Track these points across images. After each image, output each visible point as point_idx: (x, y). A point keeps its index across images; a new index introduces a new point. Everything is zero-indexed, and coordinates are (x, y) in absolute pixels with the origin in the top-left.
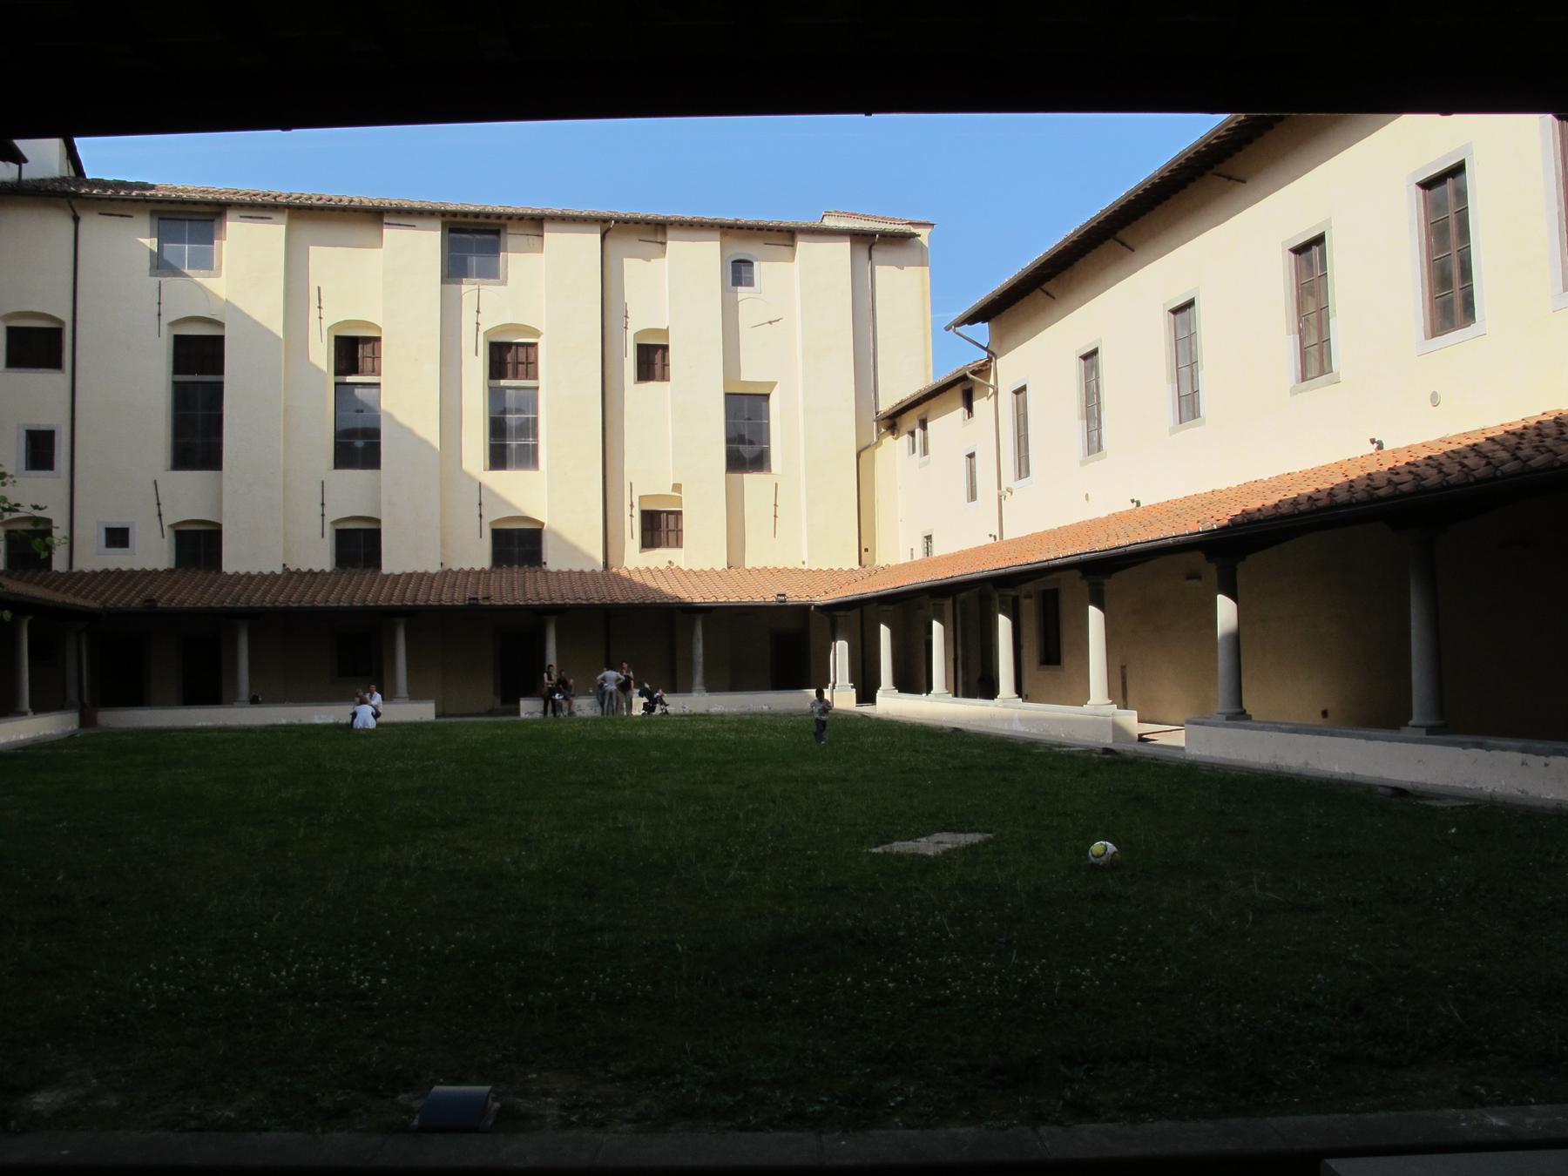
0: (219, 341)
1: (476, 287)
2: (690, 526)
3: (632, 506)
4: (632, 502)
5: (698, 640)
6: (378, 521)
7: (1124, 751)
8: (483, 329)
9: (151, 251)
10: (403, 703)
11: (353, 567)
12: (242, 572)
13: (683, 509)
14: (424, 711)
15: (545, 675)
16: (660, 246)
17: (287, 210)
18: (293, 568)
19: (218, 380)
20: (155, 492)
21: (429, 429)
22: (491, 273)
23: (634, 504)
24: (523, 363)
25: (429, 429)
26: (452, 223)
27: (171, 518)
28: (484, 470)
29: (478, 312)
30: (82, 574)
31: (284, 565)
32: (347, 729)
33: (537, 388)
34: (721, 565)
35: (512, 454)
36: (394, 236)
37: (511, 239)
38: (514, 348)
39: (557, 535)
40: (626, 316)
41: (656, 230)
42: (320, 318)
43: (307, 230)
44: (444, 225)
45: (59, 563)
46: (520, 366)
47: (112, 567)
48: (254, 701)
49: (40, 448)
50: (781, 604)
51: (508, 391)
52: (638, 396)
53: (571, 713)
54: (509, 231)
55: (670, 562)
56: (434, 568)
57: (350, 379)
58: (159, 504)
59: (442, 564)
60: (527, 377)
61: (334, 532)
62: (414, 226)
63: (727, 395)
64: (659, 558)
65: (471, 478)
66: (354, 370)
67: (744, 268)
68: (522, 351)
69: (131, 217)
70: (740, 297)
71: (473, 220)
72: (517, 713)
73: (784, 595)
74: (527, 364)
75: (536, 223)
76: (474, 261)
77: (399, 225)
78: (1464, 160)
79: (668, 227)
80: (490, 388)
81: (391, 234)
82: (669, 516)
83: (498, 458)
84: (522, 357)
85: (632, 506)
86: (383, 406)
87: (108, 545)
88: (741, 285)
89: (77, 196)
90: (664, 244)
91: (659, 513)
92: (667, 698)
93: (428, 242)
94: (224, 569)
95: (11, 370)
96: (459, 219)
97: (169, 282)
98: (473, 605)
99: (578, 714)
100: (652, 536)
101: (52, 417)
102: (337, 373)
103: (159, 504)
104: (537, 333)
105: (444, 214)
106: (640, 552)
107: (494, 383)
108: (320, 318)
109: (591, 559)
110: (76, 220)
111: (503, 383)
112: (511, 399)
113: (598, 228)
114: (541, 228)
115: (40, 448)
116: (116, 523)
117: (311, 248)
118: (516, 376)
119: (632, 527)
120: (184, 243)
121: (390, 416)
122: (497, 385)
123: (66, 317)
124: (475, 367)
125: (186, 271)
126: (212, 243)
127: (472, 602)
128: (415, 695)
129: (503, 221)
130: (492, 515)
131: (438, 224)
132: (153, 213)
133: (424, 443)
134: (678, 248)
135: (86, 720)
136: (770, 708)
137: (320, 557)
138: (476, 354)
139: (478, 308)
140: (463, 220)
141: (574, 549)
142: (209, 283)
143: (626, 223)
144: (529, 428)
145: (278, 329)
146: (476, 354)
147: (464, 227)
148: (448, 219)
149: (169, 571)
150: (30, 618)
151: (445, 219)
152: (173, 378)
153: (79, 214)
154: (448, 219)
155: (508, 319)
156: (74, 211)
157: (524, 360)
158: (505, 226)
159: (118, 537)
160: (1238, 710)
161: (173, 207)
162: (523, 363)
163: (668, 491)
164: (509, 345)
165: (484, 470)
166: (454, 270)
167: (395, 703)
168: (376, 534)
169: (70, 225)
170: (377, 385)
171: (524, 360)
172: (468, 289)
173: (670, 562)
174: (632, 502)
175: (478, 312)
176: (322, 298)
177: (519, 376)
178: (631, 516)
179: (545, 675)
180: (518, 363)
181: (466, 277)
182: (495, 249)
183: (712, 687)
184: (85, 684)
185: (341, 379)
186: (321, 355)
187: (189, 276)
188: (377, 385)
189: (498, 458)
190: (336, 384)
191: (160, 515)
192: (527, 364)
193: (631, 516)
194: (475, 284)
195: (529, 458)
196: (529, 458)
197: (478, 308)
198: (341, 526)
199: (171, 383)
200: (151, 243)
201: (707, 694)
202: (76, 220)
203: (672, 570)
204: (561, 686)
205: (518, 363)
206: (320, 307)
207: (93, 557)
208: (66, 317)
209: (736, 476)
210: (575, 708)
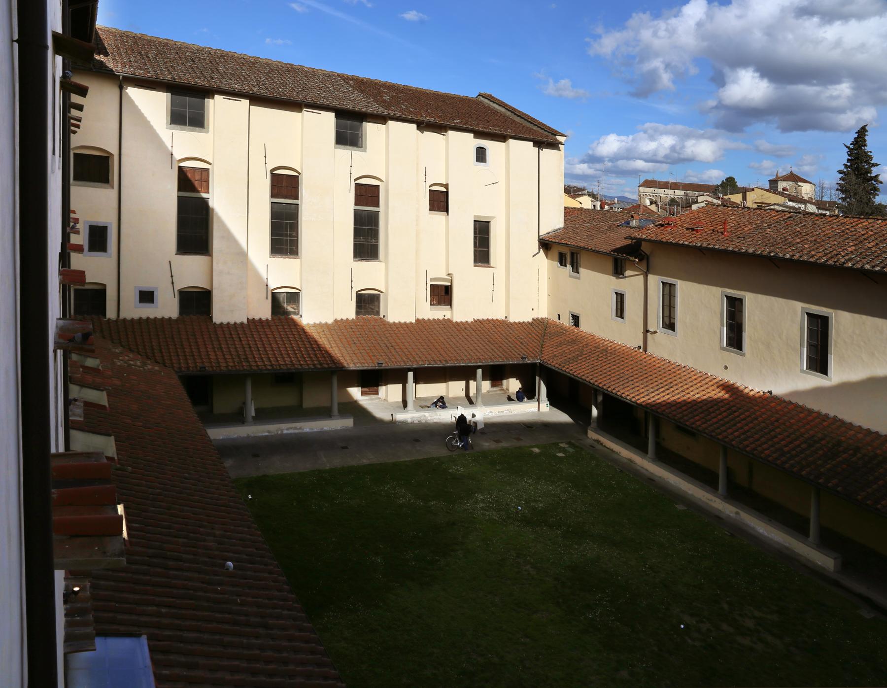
7: (213, 210)
20: (170, 268)
27: (179, 286)
30: (125, 320)
46: (740, 196)
47: (144, 316)
58: (172, 276)
63: (474, 221)
78: (560, 150)
87: (140, 302)
94: (214, 320)
103: (172, 276)
116: (147, 286)
123: (114, 151)
149: (177, 320)
152: (178, 193)
153: (123, 85)
159: (147, 297)
169: (117, 91)
177: (434, 209)
184: (229, 98)
191: (173, 283)
201: (484, 407)
207: (133, 310)
208: (115, 152)
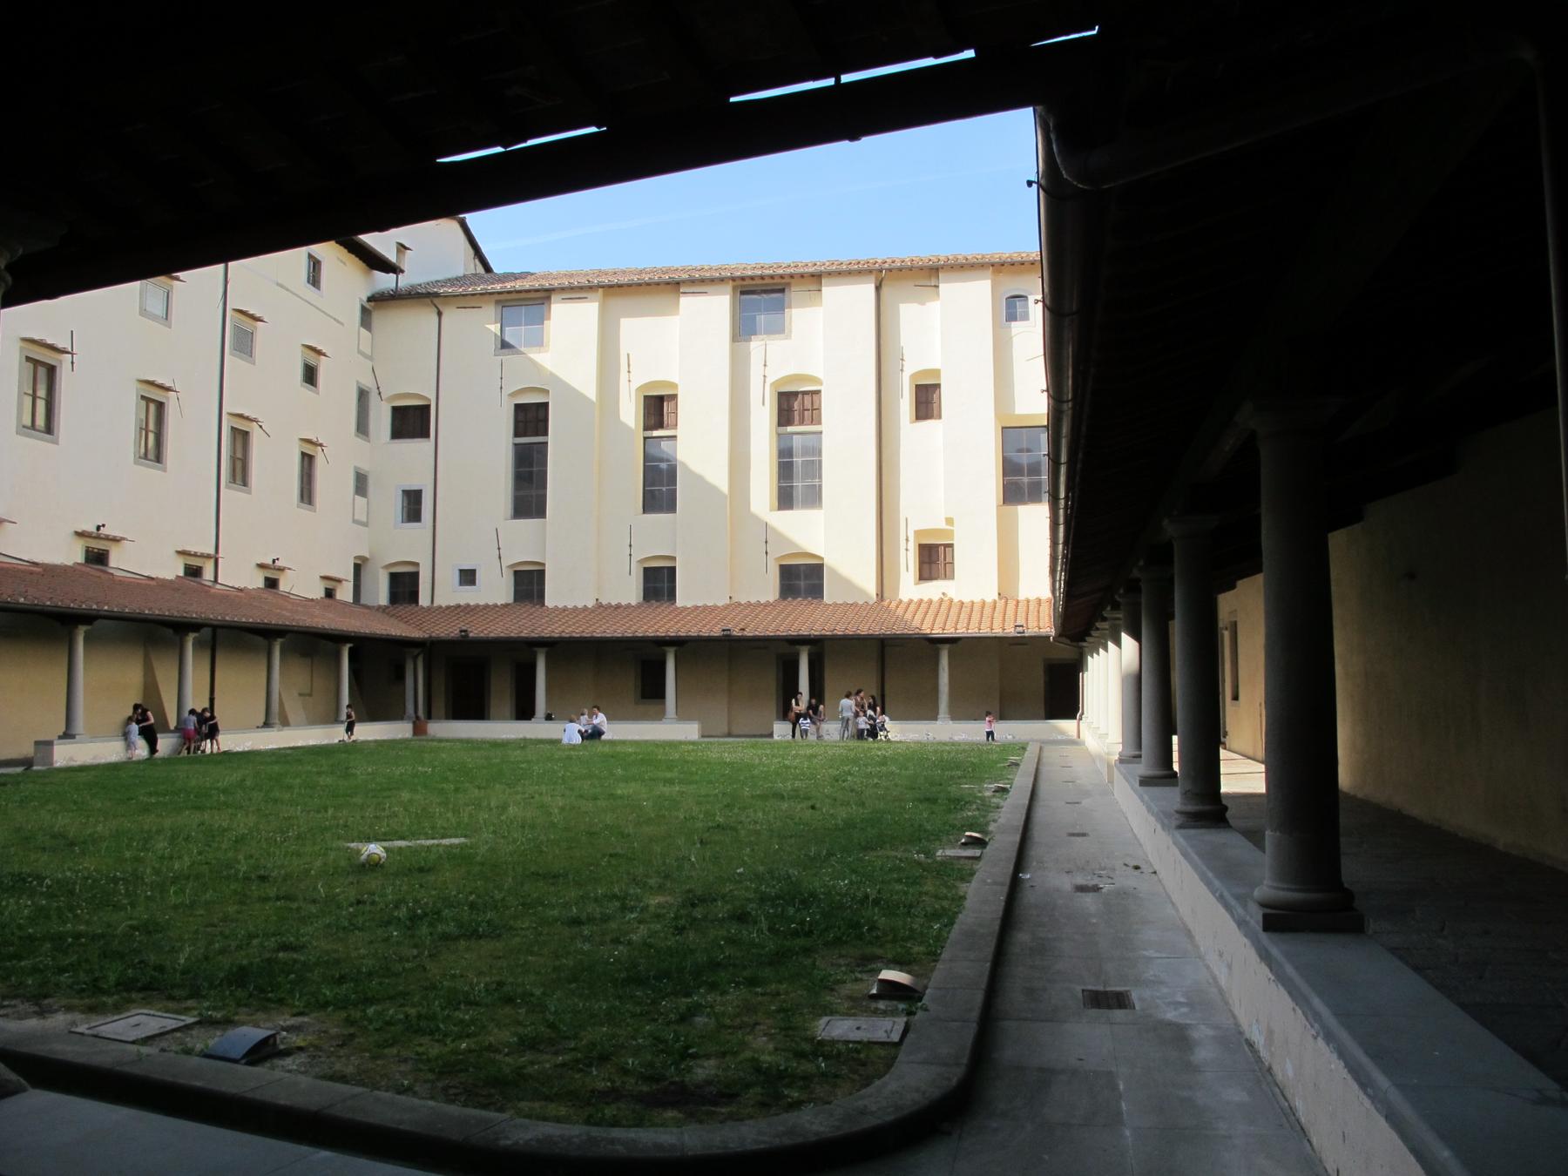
0: (544, 407)
1: (763, 342)
2: (962, 559)
3: (907, 540)
4: (907, 537)
5: (943, 669)
6: (544, 565)
8: (770, 380)
9: (496, 335)
10: (671, 723)
11: (657, 601)
12: (580, 606)
13: (955, 542)
14: (689, 731)
15: (793, 701)
16: (934, 288)
17: (600, 290)
18: (604, 603)
19: (543, 441)
21: (718, 477)
22: (779, 329)
23: (905, 541)
24: (808, 410)
25: (718, 477)
26: (741, 286)
27: (507, 561)
28: (771, 510)
29: (765, 365)
31: (597, 600)
32: (556, 742)
33: (821, 433)
34: (991, 595)
35: (798, 494)
36: (689, 303)
37: (794, 294)
38: (800, 396)
39: (833, 572)
40: (902, 360)
41: (929, 273)
42: (629, 381)
43: (617, 303)
44: (734, 288)
45: (424, 600)
46: (806, 412)
48: (549, 718)
49: (412, 504)
50: (1019, 635)
51: (794, 437)
52: (912, 434)
53: (819, 737)
54: (793, 289)
55: (944, 594)
56: (722, 602)
57: (656, 433)
59: (730, 598)
60: (811, 423)
61: (642, 570)
62: (586, 298)
64: (933, 590)
65: (756, 518)
66: (660, 425)
67: (1019, 303)
68: (807, 397)
69: (480, 307)
70: (1014, 331)
71: (760, 282)
72: (771, 735)
73: (729, 630)
74: (812, 410)
75: (815, 278)
76: (762, 319)
77: (693, 293)
79: (940, 270)
80: (779, 435)
81: (686, 302)
82: (947, 549)
83: (785, 499)
84: (808, 404)
85: (907, 540)
86: (679, 457)
88: (1015, 319)
89: (437, 295)
90: (937, 287)
91: (937, 546)
92: (889, 724)
93: (717, 307)
95: (396, 441)
96: (748, 282)
97: (508, 358)
98: (727, 636)
99: (826, 737)
100: (930, 569)
101: (421, 481)
102: (646, 428)
104: (674, 386)
105: (733, 279)
106: (916, 584)
107: (782, 429)
108: (629, 381)
109: (862, 592)
110: (440, 314)
111: (790, 429)
112: (797, 442)
113: (872, 278)
114: (549, 298)
115: (412, 504)
117: (901, 305)
118: (802, 423)
119: (908, 561)
120: (520, 325)
121: (683, 464)
122: (784, 432)
124: (763, 416)
125: (523, 349)
126: (543, 324)
127: (725, 633)
128: (682, 716)
129: (787, 280)
130: (778, 553)
131: (729, 287)
132: (497, 302)
133: (713, 489)
134: (952, 290)
135: (419, 730)
136: (1014, 737)
137: (630, 591)
138: (763, 404)
139: (765, 362)
140: (752, 282)
141: (847, 584)
142: (538, 356)
143: (1032, 264)
144: (815, 469)
145: (591, 392)
146: (763, 404)
147: (755, 288)
148: (739, 282)
150: (351, 645)
151: (735, 283)
153: (441, 309)
154: (739, 282)
155: (791, 370)
156: (438, 308)
157: (810, 407)
158: (789, 284)
159: (468, 577)
160: (1137, 753)
161: (514, 296)
162: (808, 410)
163: (942, 525)
164: (795, 394)
165: (771, 510)
166: (742, 330)
167: (664, 723)
168: (541, 573)
170: (675, 437)
171: (810, 407)
172: (756, 346)
173: (944, 594)
174: (907, 537)
175: (765, 365)
176: (631, 363)
178: (907, 550)
179: (793, 701)
180: (804, 410)
181: (756, 334)
182: (780, 308)
183: (957, 715)
185: (649, 434)
186: (630, 413)
187: (524, 354)
188: (675, 437)
189: (785, 499)
190: (645, 438)
192: (812, 410)
193: (907, 550)
194: (763, 340)
195: (814, 498)
196: (814, 498)
197: (765, 362)
198: (648, 565)
199: (511, 444)
200: (495, 328)
201: (951, 722)
202: (440, 314)
203: (946, 604)
204: (811, 712)
205: (804, 410)
206: (629, 372)
209: (1010, 508)
210: (823, 732)
